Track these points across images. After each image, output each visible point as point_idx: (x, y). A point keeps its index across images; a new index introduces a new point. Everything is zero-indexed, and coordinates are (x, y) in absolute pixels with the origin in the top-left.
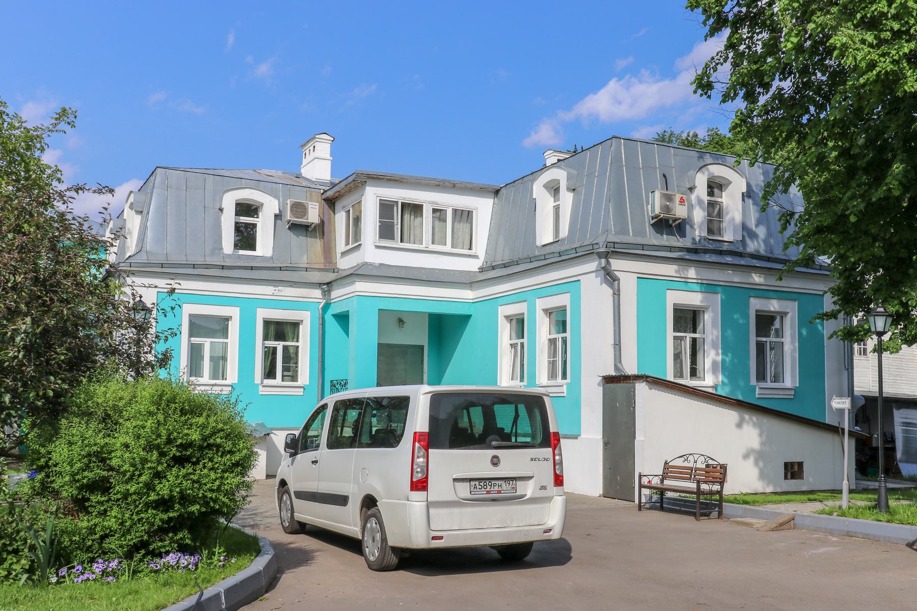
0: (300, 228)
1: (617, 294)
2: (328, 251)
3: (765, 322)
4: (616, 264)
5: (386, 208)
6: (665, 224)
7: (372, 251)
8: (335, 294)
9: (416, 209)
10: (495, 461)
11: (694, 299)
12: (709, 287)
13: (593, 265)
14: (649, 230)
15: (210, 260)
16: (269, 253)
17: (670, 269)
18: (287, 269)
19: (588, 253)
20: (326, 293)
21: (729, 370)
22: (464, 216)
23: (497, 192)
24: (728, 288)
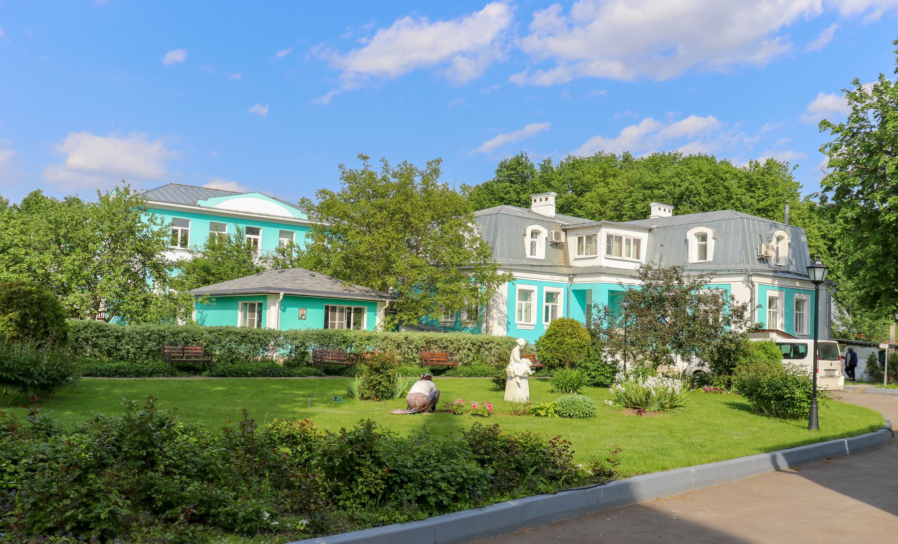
0: (555, 245)
1: (752, 292)
2: (566, 256)
3: (799, 303)
4: (754, 279)
5: (609, 237)
6: (763, 259)
7: (602, 260)
8: (575, 280)
9: (619, 239)
10: (302, 317)
11: (775, 294)
12: (781, 288)
13: (742, 278)
14: (757, 261)
15: (519, 262)
16: (543, 257)
17: (769, 281)
18: (556, 266)
19: (740, 272)
20: (571, 279)
21: (785, 325)
22: (637, 242)
23: (650, 230)
24: (788, 288)
